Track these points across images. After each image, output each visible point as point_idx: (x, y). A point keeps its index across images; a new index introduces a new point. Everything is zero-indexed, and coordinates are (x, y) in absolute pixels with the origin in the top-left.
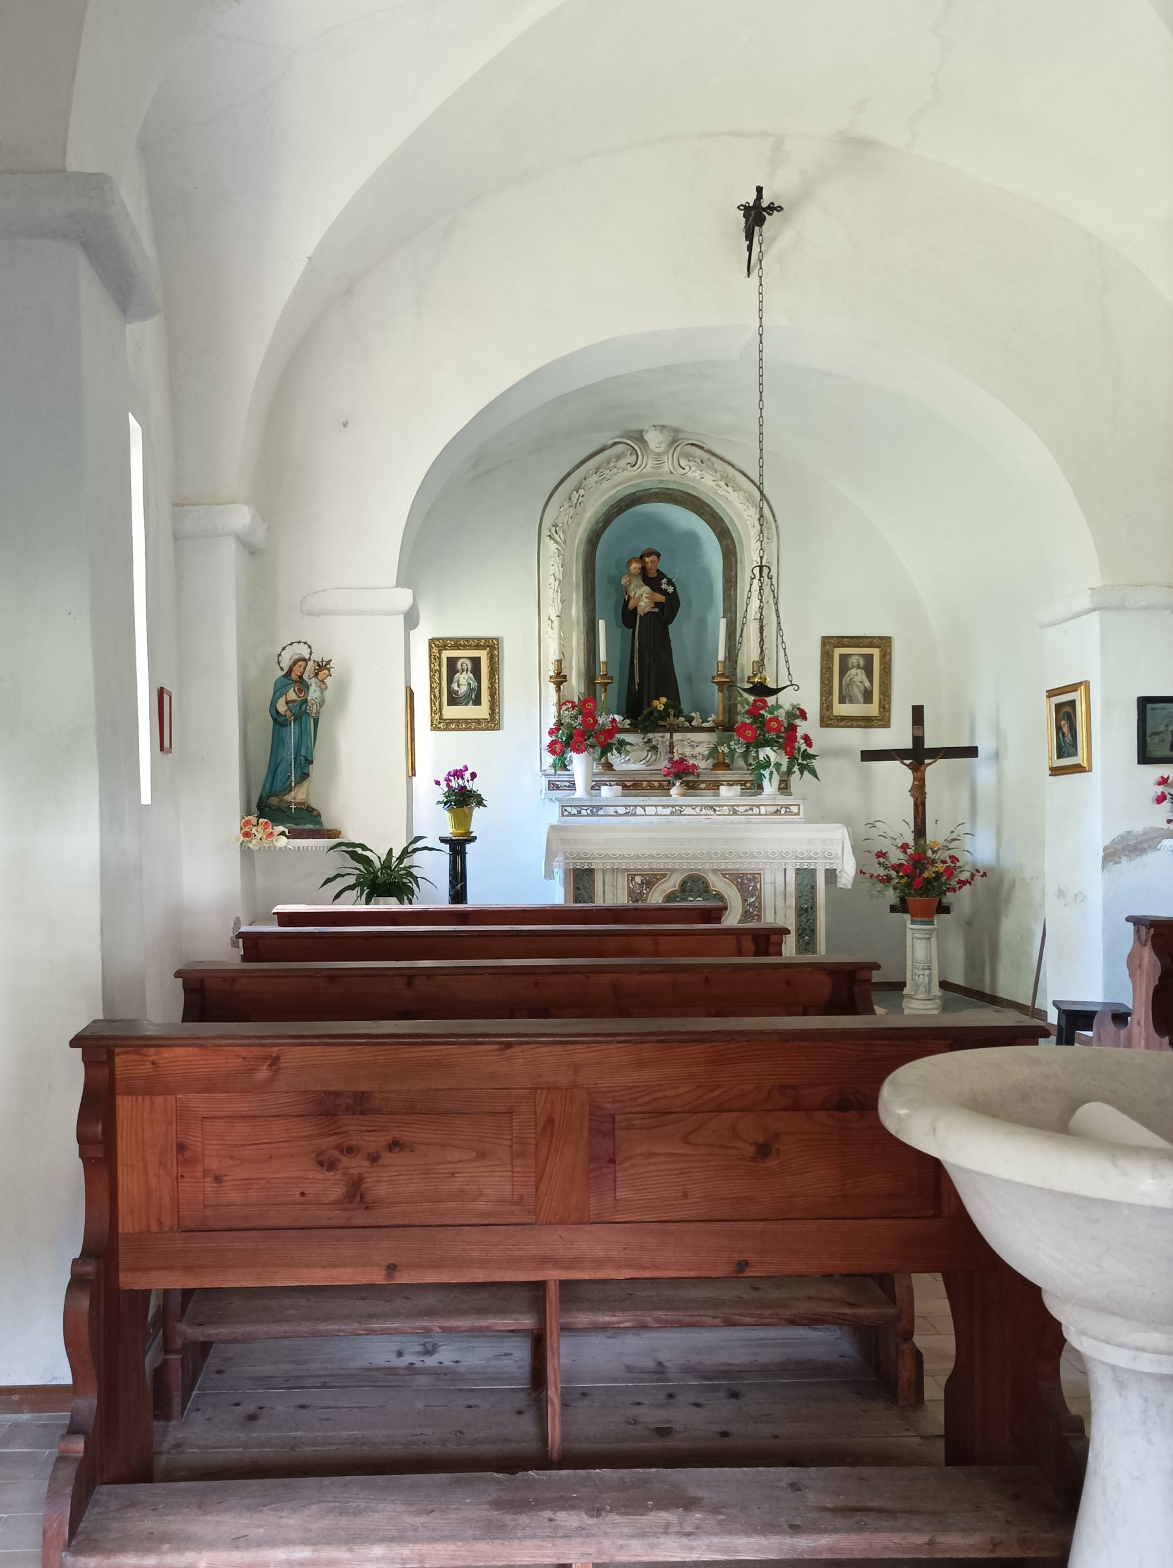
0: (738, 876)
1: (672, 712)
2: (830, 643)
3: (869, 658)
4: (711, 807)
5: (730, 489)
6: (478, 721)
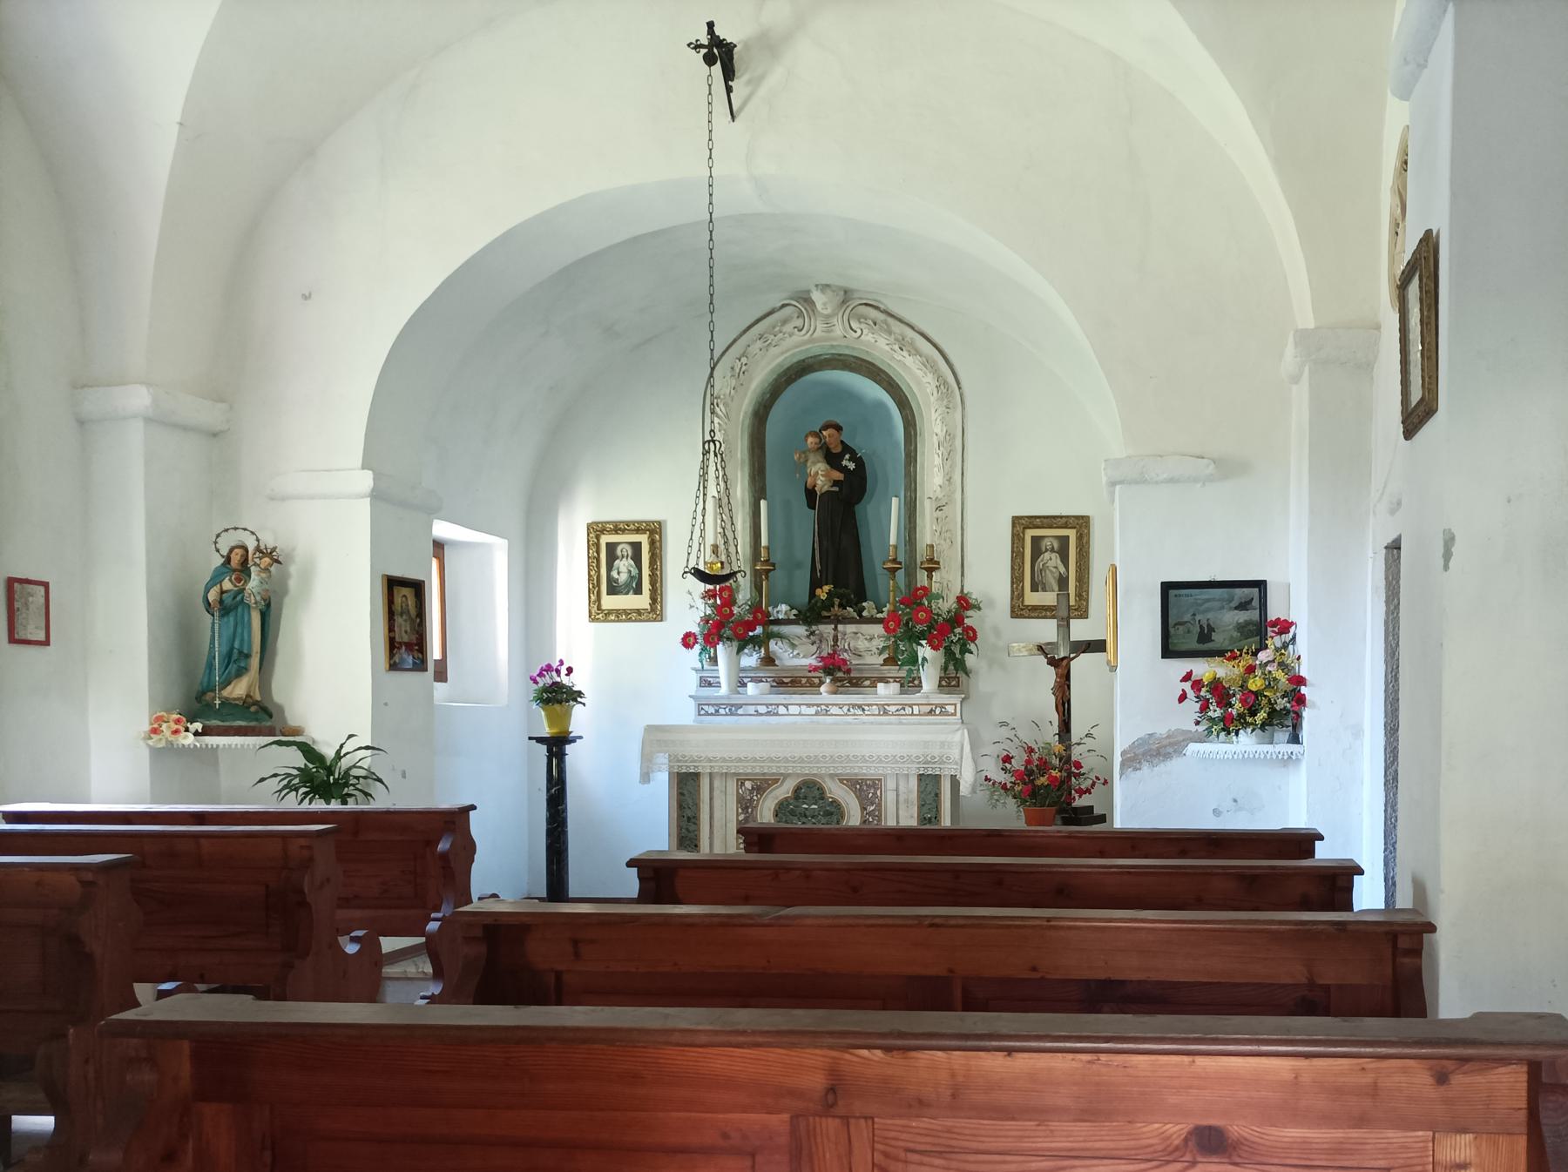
0: (857, 782)
1: (837, 601)
2: (1021, 524)
3: (1064, 541)
4: (860, 706)
5: (905, 353)
6: (638, 612)
